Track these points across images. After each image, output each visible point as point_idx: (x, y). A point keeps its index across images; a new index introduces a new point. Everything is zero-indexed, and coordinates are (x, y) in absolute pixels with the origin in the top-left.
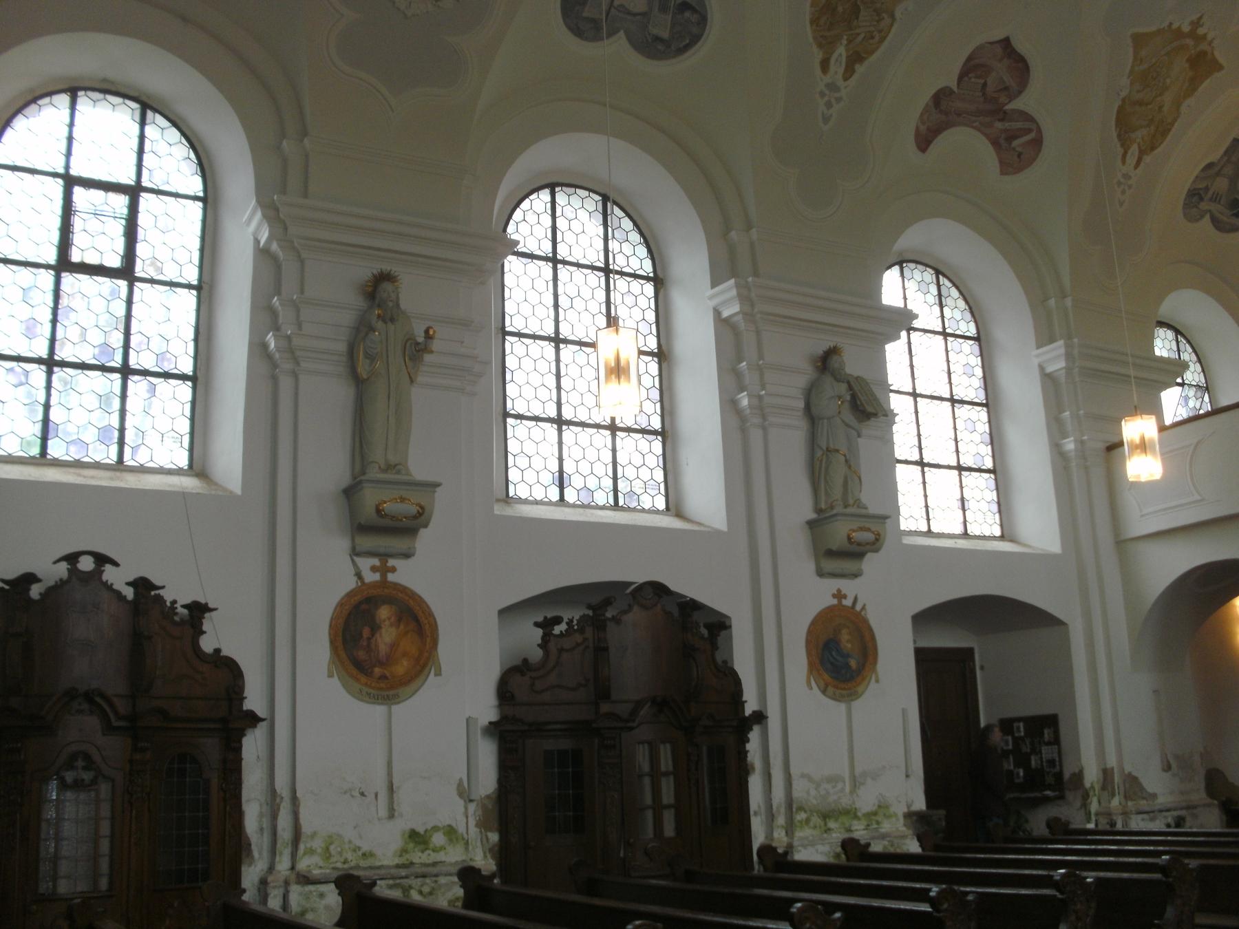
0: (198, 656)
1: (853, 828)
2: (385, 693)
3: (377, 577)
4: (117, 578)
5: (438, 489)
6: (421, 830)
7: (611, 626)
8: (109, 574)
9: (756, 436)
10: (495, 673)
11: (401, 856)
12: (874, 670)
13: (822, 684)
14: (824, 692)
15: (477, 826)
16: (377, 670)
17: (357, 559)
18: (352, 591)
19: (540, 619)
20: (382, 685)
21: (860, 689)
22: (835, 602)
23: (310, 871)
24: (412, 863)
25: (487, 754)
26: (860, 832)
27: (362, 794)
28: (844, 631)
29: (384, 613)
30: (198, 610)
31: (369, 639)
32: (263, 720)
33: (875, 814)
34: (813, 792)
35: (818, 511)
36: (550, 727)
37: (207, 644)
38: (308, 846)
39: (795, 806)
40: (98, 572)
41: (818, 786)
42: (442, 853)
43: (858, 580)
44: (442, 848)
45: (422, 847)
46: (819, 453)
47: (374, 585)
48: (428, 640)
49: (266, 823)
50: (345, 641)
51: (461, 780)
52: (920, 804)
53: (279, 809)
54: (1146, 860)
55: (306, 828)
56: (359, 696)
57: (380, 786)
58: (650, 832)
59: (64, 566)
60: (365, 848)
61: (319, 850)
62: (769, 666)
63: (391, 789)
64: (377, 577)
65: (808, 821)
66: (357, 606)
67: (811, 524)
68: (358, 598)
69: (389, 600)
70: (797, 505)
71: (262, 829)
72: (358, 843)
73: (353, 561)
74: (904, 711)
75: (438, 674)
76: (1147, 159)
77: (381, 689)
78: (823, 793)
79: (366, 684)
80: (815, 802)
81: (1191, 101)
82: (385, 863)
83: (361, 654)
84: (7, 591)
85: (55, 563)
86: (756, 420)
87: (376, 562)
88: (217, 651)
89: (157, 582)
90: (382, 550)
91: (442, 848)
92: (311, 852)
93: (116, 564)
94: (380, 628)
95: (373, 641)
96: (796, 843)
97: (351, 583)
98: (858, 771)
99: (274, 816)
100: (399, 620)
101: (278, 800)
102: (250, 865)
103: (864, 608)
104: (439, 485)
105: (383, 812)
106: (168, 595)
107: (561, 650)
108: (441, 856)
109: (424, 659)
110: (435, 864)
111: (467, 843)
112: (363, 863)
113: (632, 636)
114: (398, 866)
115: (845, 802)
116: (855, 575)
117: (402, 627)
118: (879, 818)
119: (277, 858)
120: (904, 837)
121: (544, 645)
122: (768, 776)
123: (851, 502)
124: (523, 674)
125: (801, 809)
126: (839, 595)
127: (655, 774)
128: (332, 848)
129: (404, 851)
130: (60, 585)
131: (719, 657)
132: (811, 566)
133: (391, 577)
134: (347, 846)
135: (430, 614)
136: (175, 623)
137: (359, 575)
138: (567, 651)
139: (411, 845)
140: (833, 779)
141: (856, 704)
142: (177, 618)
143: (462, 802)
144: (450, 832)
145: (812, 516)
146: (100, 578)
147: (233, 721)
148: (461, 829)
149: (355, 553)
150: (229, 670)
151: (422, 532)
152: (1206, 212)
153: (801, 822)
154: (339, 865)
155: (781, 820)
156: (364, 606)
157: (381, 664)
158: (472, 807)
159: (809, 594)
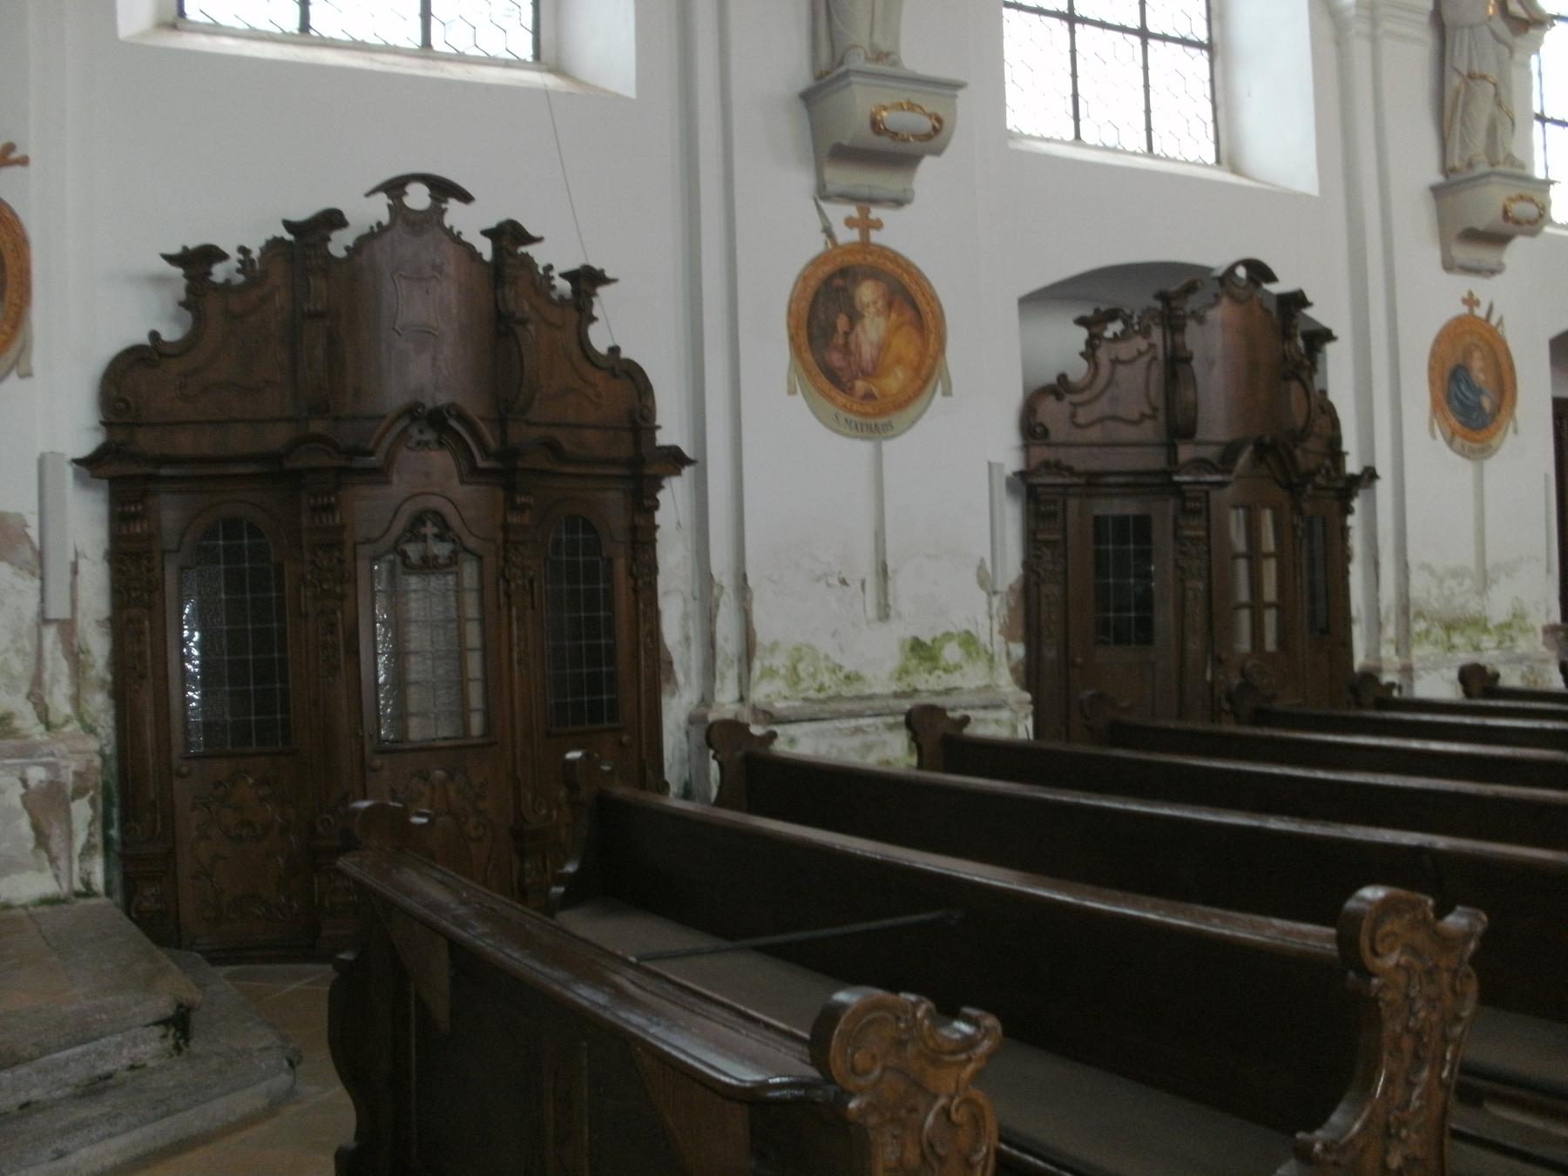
0: (588, 358)
1: (1482, 646)
2: (872, 421)
3: (853, 235)
4: (469, 222)
5: (961, 93)
6: (926, 638)
7: (1191, 325)
8: (456, 215)
9: (1360, 50)
10: (1014, 399)
11: (900, 679)
12: (1511, 414)
13: (1449, 432)
14: (1450, 443)
15: (1000, 632)
16: (860, 385)
17: (823, 204)
18: (818, 257)
19: (1088, 312)
20: (869, 409)
21: (1494, 443)
22: (1464, 310)
23: (771, 704)
24: (916, 691)
25: (1012, 517)
26: (1490, 655)
27: (843, 582)
28: (1477, 355)
29: (867, 293)
30: (588, 280)
31: (846, 334)
32: (689, 462)
33: (1509, 625)
34: (1435, 591)
35: (1447, 170)
36: (1112, 480)
37: (600, 338)
38: (767, 663)
39: (1412, 611)
40: (436, 212)
41: (1441, 581)
42: (957, 675)
43: (1498, 278)
44: (958, 667)
45: (928, 665)
46: (1454, 81)
47: (851, 249)
48: (932, 338)
49: (694, 630)
50: (811, 338)
51: (982, 560)
52: (1556, 617)
53: (718, 606)
55: (763, 636)
56: (834, 425)
57: (865, 567)
58: (1244, 645)
59: (381, 203)
60: (849, 667)
61: (782, 671)
62: (1376, 398)
63: (883, 572)
64: (853, 235)
65: (1428, 632)
66: (827, 282)
67: (1437, 191)
68: (827, 269)
69: (874, 274)
70: (1416, 161)
71: (687, 638)
72: (838, 659)
73: (818, 207)
74: (1546, 476)
75: (947, 392)
77: (866, 415)
78: (1447, 592)
79: (844, 407)
80: (1436, 605)
82: (879, 689)
83: (836, 359)
84: (290, 242)
85: (368, 195)
86: (1363, 27)
87: (852, 211)
88: (614, 350)
89: (532, 230)
90: (865, 192)
91: (958, 667)
92: (770, 673)
93: (465, 197)
94: (862, 316)
95: (852, 338)
96: (1417, 665)
97: (816, 245)
98: (1489, 562)
99: (710, 618)
100: (890, 305)
101: (716, 591)
102: (673, 694)
103: (1500, 322)
104: (957, 86)
105: (872, 612)
106: (539, 255)
107: (1115, 362)
108: (955, 680)
109: (926, 371)
110: (948, 691)
111: (991, 659)
112: (846, 691)
113: (1213, 339)
114: (896, 695)
115: (1474, 606)
116: (1492, 272)
117: (894, 316)
118: (1514, 633)
119: (718, 684)
120: (1545, 661)
121: (1090, 353)
122: (1375, 564)
123: (1501, 157)
124: (1059, 397)
125: (1420, 615)
126: (1471, 301)
127: (1254, 556)
128: (801, 667)
129: (904, 671)
130: (376, 233)
131: (1318, 385)
132: (1435, 255)
133: (876, 237)
134: (823, 664)
135: (933, 299)
136: (551, 301)
137: (828, 231)
138: (1124, 363)
139: (914, 662)
140: (1458, 574)
141: (1491, 464)
142: (554, 295)
143: (983, 595)
144: (968, 641)
145: (1437, 178)
146: (441, 224)
147: (645, 465)
148: (984, 638)
149: (823, 194)
150: (629, 378)
151: (928, 163)
153: (1419, 634)
154: (812, 694)
155: (1390, 631)
156: (839, 282)
157: (866, 375)
158: (996, 601)
159: (1432, 297)
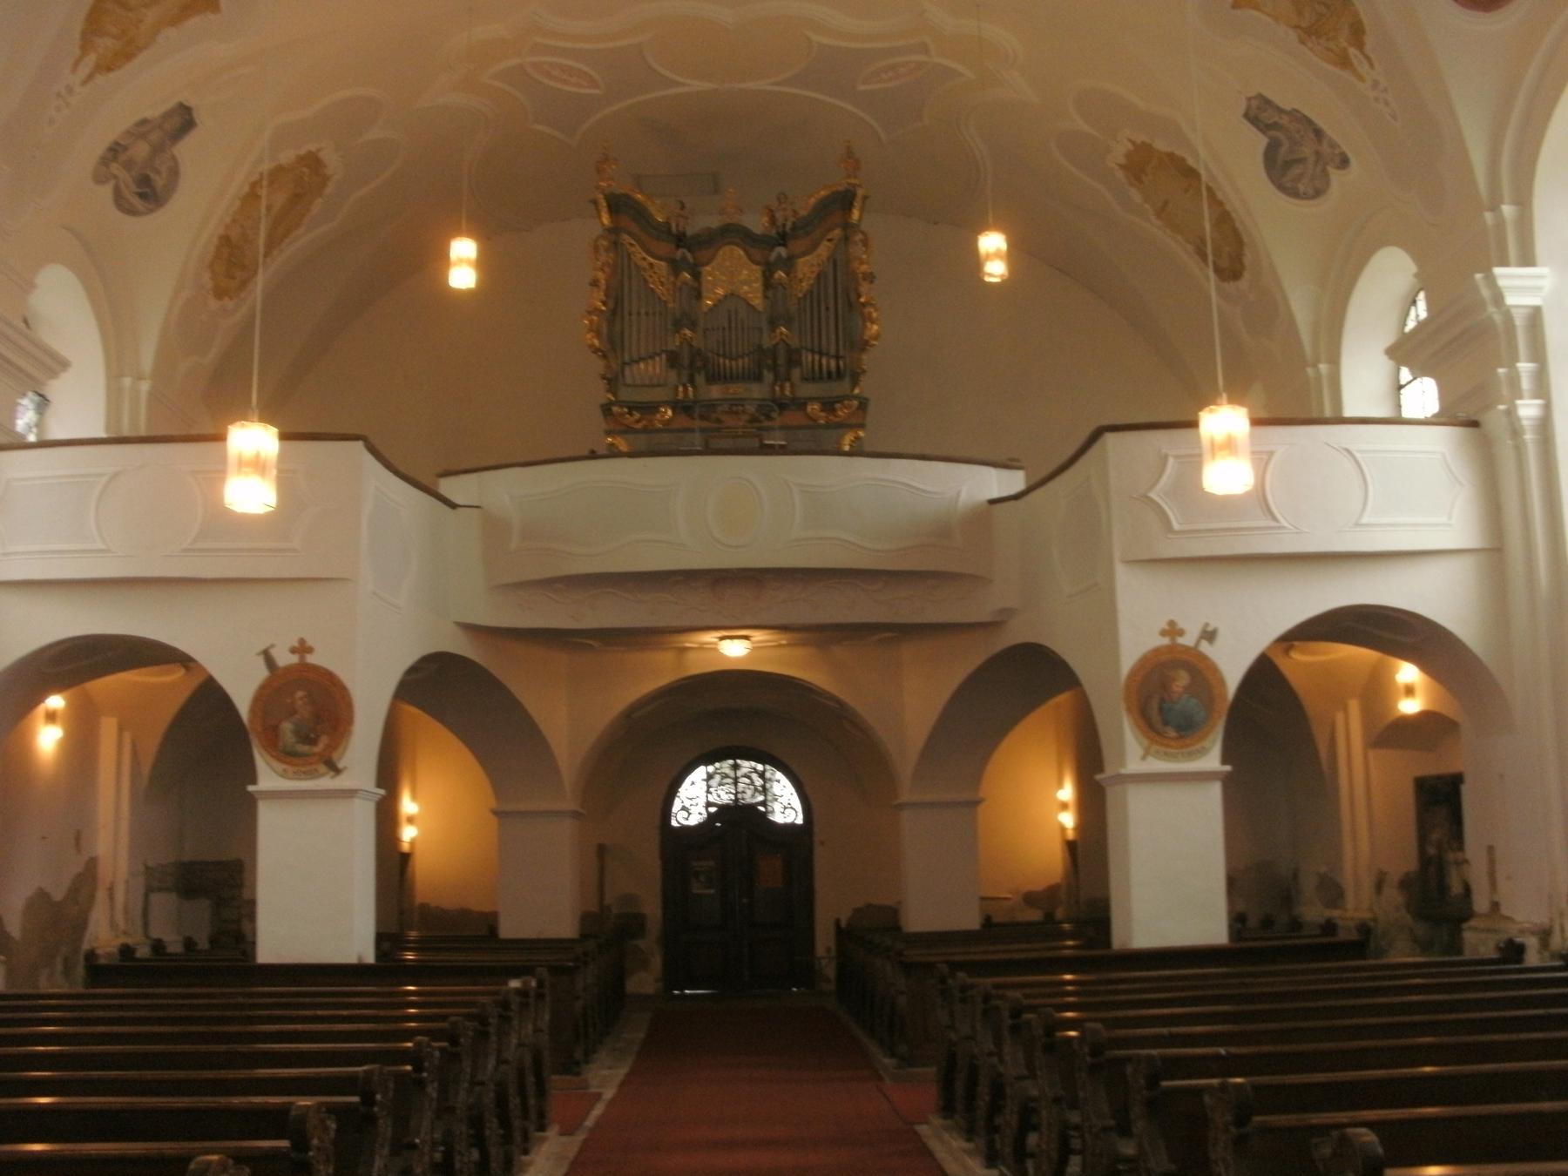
22: (1166, 641)
54: (171, 1048)
76: (100, 79)
81: (170, 32)
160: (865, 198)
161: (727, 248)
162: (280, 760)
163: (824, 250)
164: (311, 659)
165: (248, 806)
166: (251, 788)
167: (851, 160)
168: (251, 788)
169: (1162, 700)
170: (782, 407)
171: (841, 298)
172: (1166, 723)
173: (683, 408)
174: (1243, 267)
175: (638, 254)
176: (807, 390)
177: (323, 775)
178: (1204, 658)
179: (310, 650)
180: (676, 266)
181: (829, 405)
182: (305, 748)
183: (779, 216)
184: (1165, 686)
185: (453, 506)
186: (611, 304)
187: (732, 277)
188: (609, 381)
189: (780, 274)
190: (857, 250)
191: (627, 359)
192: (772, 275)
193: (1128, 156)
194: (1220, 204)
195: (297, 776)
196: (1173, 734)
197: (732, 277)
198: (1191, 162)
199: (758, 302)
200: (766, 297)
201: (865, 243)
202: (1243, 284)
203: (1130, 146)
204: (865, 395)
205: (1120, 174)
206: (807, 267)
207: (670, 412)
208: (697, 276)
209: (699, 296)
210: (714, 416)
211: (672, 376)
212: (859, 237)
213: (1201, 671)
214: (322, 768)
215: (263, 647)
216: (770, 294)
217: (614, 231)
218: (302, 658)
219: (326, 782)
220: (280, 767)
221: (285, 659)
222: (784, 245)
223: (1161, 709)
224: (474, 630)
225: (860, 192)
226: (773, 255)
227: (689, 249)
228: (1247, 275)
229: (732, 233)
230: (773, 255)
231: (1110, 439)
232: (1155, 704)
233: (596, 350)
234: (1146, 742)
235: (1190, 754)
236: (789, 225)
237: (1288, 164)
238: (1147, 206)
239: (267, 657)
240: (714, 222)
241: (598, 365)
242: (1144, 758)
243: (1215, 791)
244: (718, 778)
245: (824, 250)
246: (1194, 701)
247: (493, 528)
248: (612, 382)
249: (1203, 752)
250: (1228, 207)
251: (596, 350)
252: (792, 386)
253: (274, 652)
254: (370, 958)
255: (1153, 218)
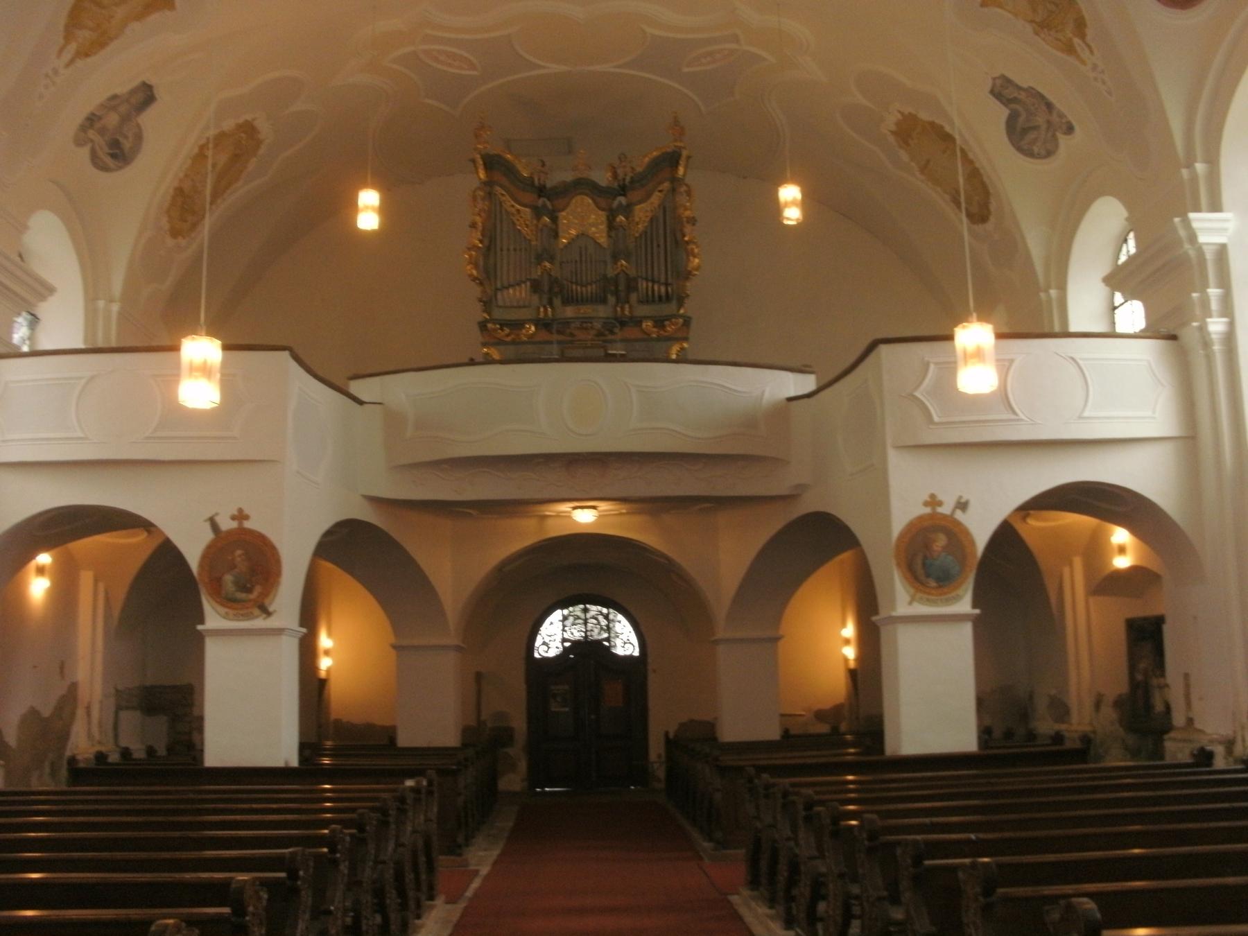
22: (928, 510)
76: (80, 63)
81: (136, 26)
152: (92, 141)
160: (689, 157)
161: (579, 197)
162: (223, 605)
163: (656, 199)
164: (248, 525)
165: (197, 642)
166: (200, 627)
167: (677, 127)
168: (200, 627)
169: (925, 557)
170: (623, 324)
171: (669, 238)
172: (928, 576)
173: (544, 325)
174: (989, 213)
175: (508, 202)
176: (642, 310)
177: (257, 617)
178: (959, 524)
179: (247, 518)
180: (538, 212)
181: (660, 322)
182: (243, 596)
183: (620, 172)
184: (927, 546)
185: (361, 403)
186: (486, 242)
187: (582, 221)
188: (485, 303)
189: (621, 218)
190: (682, 199)
191: (499, 285)
192: (614, 219)
193: (898, 124)
194: (971, 162)
195: (237, 618)
196: (933, 584)
197: (582, 221)
198: (948, 129)
199: (603, 240)
200: (609, 236)
201: (689, 193)
202: (989, 226)
203: (899, 116)
204: (689, 314)
205: (891, 139)
206: (643, 213)
207: (533, 328)
208: (554, 219)
209: (556, 236)
210: (568, 331)
211: (535, 299)
212: (683, 189)
213: (956, 534)
214: (257, 611)
215: (209, 515)
216: (613, 234)
217: (489, 184)
218: (241, 523)
219: (260, 623)
220: (223, 610)
221: (227, 524)
222: (624, 195)
223: (924, 564)
224: (377, 502)
225: (685, 153)
226: (616, 203)
227: (549, 198)
228: (992, 219)
229: (583, 186)
230: (616, 203)
231: (884, 349)
232: (919, 561)
233: (474, 279)
234: (912, 591)
235: (947, 600)
236: (628, 179)
237: (1025, 131)
238: (913, 164)
239: (213, 523)
240: (569, 177)
241: (476, 291)
242: (910, 603)
243: (967, 630)
244: (571, 619)
245: (656, 199)
246: (950, 558)
247: (393, 421)
248: (487, 304)
249: (958, 598)
250: (977, 165)
251: (474, 279)
252: (631, 307)
253: (218, 519)
254: (294, 763)
255: (918, 174)
